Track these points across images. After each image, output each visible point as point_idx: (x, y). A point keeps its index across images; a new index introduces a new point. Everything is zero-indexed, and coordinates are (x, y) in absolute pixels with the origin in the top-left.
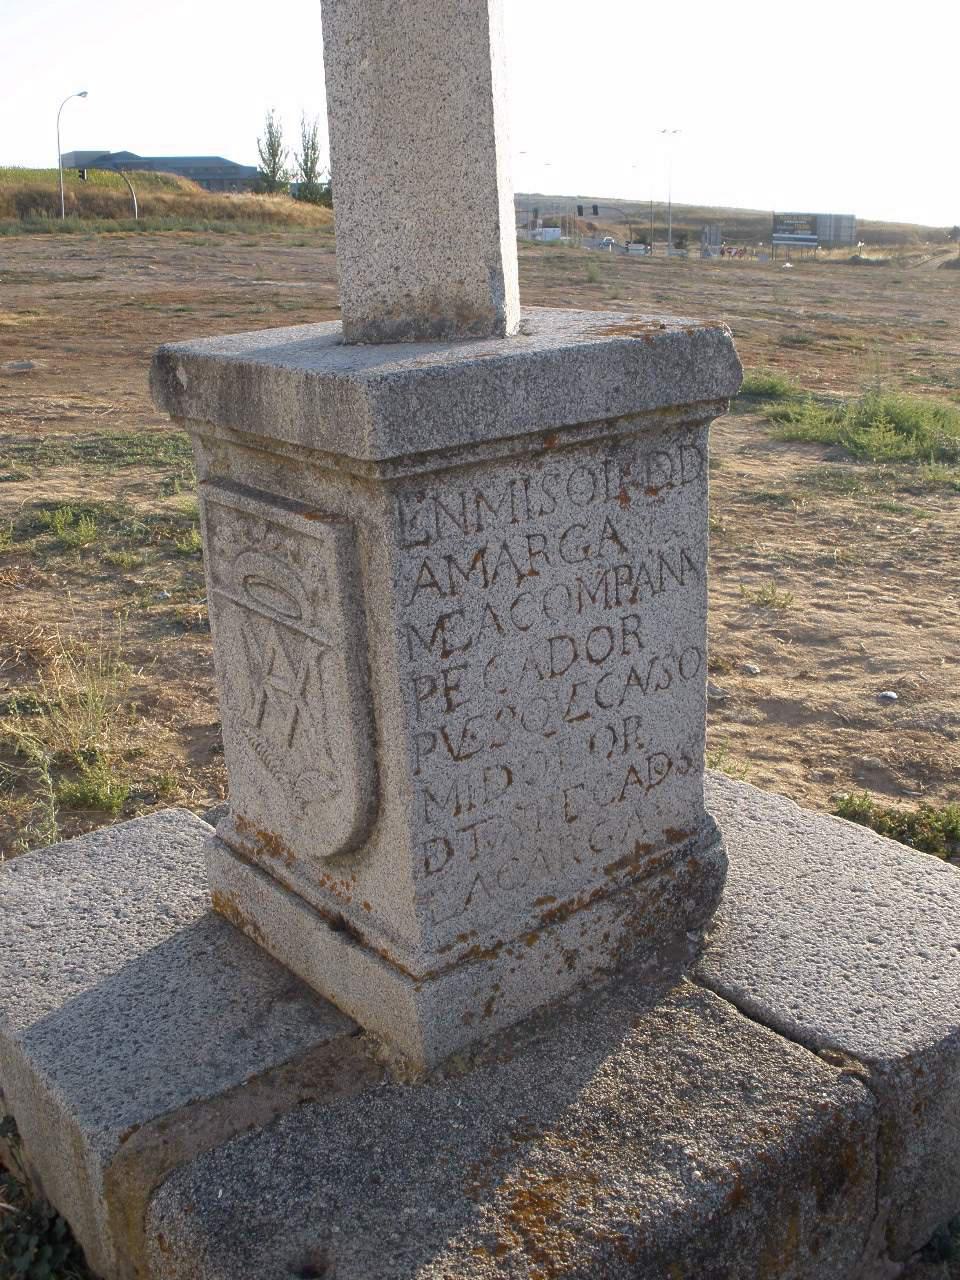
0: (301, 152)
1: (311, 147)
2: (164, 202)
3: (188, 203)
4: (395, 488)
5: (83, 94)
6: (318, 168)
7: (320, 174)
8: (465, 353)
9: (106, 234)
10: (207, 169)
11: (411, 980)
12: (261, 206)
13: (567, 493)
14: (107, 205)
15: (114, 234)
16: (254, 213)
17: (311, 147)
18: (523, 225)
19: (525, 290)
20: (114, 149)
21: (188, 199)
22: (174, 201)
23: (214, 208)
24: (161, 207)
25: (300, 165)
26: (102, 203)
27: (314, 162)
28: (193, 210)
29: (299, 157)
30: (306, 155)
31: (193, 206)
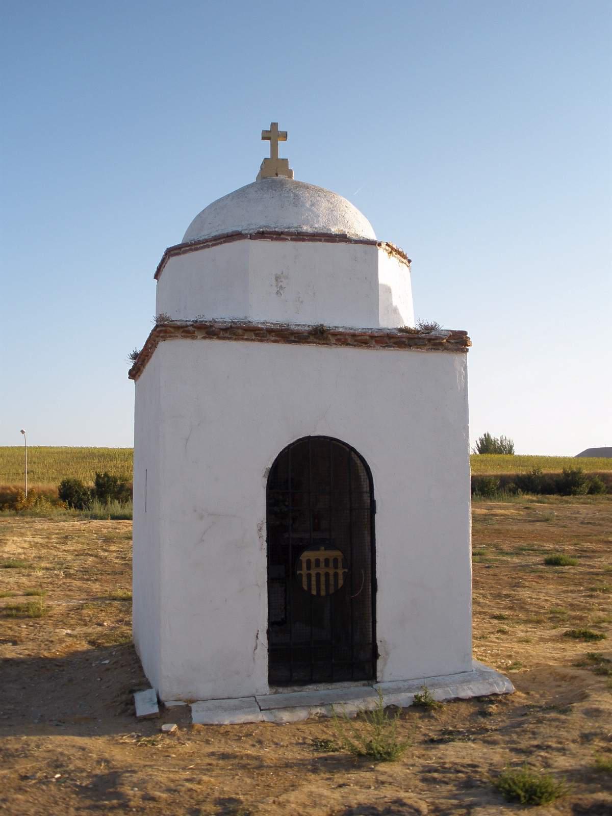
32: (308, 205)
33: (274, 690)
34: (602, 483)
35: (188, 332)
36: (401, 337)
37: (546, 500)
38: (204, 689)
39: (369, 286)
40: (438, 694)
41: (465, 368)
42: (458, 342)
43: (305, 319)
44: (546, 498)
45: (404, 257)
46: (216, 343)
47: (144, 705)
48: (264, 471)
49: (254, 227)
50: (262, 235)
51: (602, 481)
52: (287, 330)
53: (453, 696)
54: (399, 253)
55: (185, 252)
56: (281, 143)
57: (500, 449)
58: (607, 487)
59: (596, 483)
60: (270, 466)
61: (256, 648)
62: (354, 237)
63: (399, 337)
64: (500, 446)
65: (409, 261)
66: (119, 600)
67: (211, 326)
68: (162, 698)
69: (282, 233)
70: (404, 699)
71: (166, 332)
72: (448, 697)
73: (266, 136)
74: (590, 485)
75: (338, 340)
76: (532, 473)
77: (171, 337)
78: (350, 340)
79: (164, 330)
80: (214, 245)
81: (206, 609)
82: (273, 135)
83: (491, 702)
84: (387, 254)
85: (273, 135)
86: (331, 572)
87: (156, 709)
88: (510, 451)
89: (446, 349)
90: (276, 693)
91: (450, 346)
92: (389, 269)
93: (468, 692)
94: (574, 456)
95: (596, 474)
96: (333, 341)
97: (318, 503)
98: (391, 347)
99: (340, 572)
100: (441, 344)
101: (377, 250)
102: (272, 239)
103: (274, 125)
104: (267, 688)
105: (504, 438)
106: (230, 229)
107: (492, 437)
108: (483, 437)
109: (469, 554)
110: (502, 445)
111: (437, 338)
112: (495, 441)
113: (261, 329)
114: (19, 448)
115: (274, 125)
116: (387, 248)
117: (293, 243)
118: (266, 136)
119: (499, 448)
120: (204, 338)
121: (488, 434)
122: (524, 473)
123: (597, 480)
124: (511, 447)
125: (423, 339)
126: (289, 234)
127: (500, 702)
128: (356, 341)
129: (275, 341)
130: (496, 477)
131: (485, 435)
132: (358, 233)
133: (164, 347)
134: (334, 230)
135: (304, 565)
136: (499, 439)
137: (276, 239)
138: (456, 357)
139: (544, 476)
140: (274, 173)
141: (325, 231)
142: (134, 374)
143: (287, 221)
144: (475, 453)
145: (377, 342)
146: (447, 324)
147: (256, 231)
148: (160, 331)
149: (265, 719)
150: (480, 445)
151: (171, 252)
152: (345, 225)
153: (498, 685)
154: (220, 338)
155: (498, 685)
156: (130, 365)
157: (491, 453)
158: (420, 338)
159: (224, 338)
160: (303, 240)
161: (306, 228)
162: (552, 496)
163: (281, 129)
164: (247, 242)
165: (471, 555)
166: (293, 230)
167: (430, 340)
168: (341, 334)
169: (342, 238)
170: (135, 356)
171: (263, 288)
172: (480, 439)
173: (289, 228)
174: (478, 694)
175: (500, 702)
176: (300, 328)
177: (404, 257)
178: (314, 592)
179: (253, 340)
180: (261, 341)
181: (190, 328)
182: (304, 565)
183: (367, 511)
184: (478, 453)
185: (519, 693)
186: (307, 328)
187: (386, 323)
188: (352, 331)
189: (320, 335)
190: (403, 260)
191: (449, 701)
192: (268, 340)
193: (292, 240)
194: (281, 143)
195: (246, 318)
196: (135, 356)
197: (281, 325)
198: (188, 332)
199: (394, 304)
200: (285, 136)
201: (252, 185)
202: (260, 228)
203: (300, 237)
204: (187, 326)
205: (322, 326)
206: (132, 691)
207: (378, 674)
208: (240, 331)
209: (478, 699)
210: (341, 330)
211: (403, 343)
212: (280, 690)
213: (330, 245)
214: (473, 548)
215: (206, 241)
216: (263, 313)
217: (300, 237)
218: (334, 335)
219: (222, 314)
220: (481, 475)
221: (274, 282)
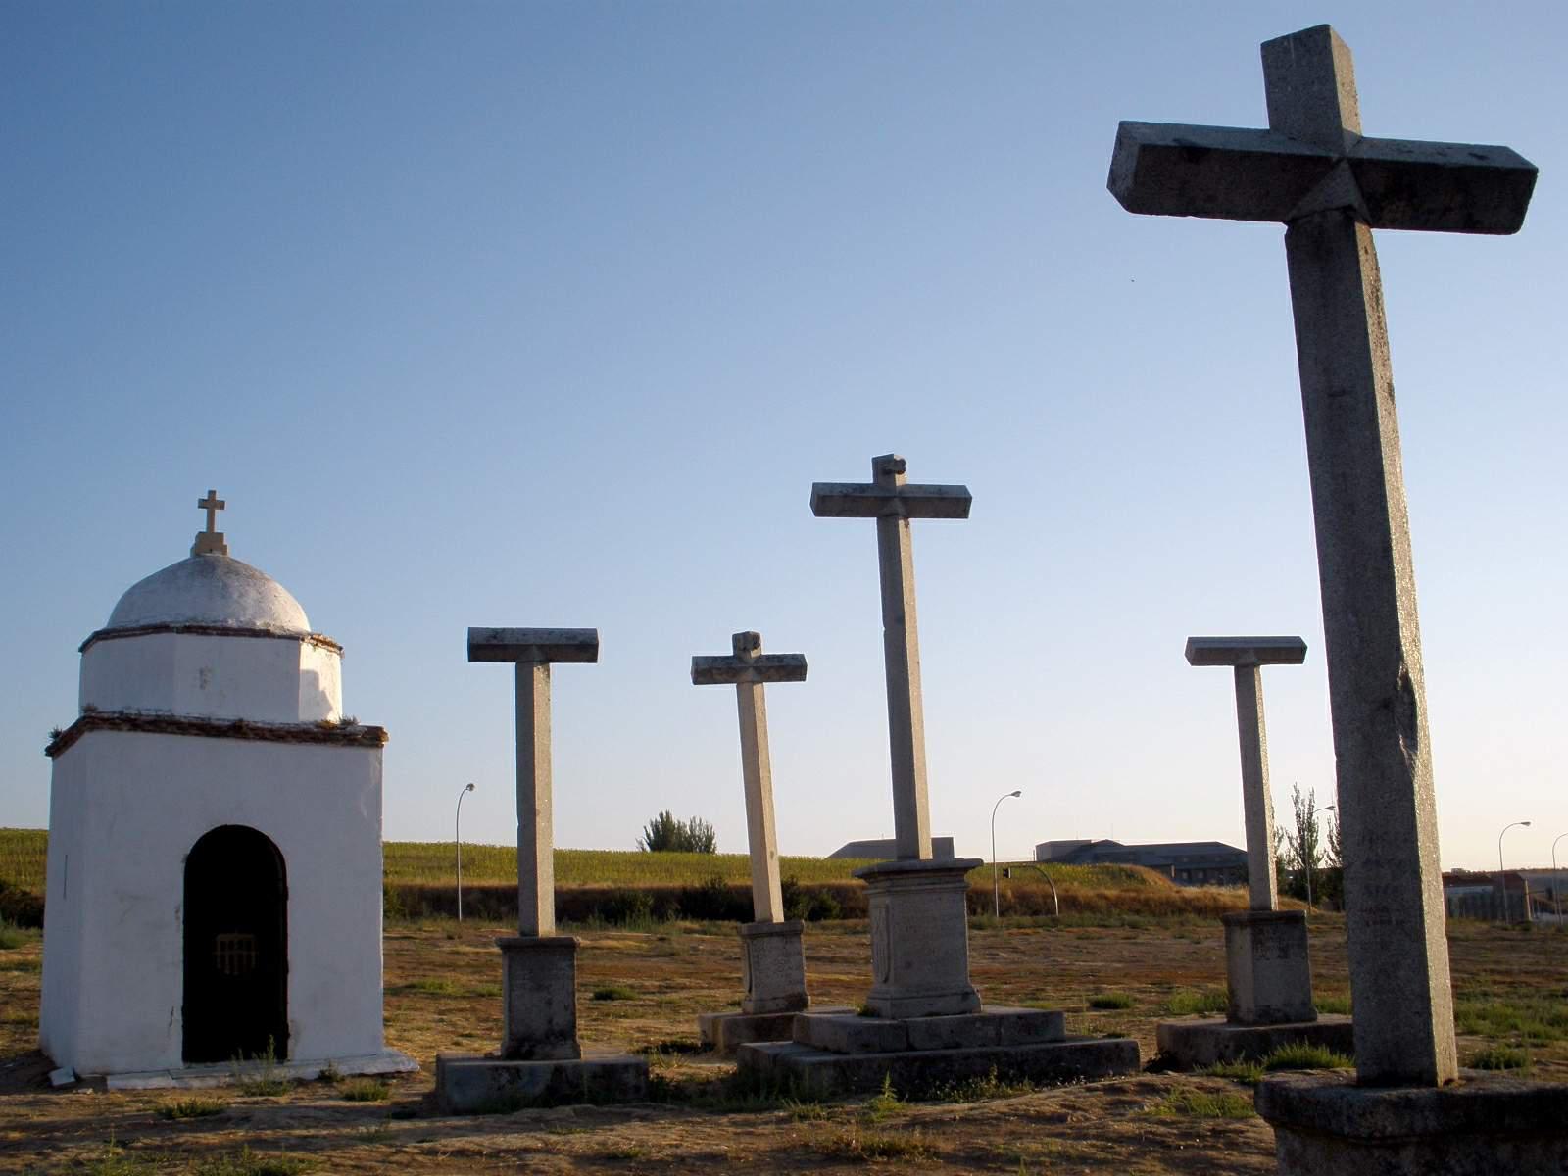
0: (1295, 833)
1: (1307, 828)
2: (1106, 898)
3: (1134, 899)
4: (751, 938)
5: (1017, 794)
6: (1318, 851)
7: (1319, 860)
8: (1310, 1024)
9: (1015, 931)
10: (1203, 857)
11: (830, 1046)
12: (1215, 899)
13: (776, 941)
14: (1045, 903)
15: (1022, 931)
16: (1207, 907)
17: (1307, 828)
18: (1456, 909)
19: (1457, 975)
20: (1095, 837)
21: (1133, 894)
22: (1118, 897)
23: (1162, 903)
24: (1102, 903)
25: (1296, 849)
26: (1040, 900)
27: (1312, 847)
28: (1138, 907)
29: (1294, 841)
30: (1302, 838)
31: (1139, 901)
32: (236, 596)
33: (187, 1066)
34: (835, 903)
35: (114, 724)
36: (317, 733)
37: (714, 930)
38: (119, 1064)
39: (291, 677)
40: (343, 1070)
41: (381, 764)
42: (374, 737)
43: (226, 714)
44: (716, 926)
45: (333, 645)
46: (141, 736)
47: (58, 1078)
48: (182, 856)
49: (181, 620)
50: (188, 630)
51: (834, 898)
52: (209, 724)
53: (358, 1072)
54: (325, 643)
55: (114, 637)
56: (217, 512)
57: (690, 843)
58: (842, 909)
59: (823, 902)
60: (189, 852)
61: (170, 1024)
62: (278, 632)
63: (314, 733)
64: (690, 837)
65: (341, 648)
66: (11, 1024)
67: (136, 720)
68: (78, 1071)
69: (208, 628)
70: (311, 1072)
71: (93, 723)
72: (353, 1072)
73: (203, 504)
74: (810, 907)
75: (256, 735)
76: (710, 885)
77: (98, 728)
78: (267, 735)
79: (91, 721)
80: (141, 635)
81: (117, 990)
82: (211, 504)
83: (394, 1078)
84: (311, 647)
85: (211, 504)
86: (245, 953)
87: (73, 1079)
88: (707, 845)
89: (361, 744)
90: (189, 1068)
91: (365, 741)
92: (311, 658)
93: (373, 1069)
94: (826, 857)
95: (822, 887)
96: (251, 736)
97: (235, 891)
98: (306, 741)
99: (253, 954)
100: (355, 740)
101: (300, 645)
102: (198, 633)
103: (212, 493)
104: (181, 1064)
105: (697, 822)
106: (157, 621)
107: (675, 820)
108: (659, 820)
109: (379, 940)
110: (693, 835)
111: (351, 734)
112: (679, 826)
113: (182, 723)
114: (446, 846)
115: (212, 493)
116: (312, 641)
117: (218, 637)
118: (203, 504)
119: (688, 840)
120: (130, 730)
121: (668, 814)
122: (697, 885)
123: (826, 897)
124: (710, 839)
125: (337, 734)
126: (215, 629)
127: (402, 1078)
128: (274, 735)
129: (197, 735)
130: (648, 892)
131: (661, 816)
132: (285, 625)
133: (88, 738)
134: (259, 624)
135: (219, 947)
136: (688, 824)
137: (202, 634)
138: (372, 752)
139: (729, 891)
140: (209, 543)
141: (248, 627)
142: (52, 751)
143: (214, 614)
144: (643, 849)
145: (294, 737)
146: (365, 721)
147: (183, 625)
148: (88, 723)
149: (177, 1085)
150: (652, 835)
151: (99, 636)
152: (272, 617)
153: (403, 1064)
154: (144, 730)
155: (403, 1064)
156: (49, 742)
157: (674, 850)
158: (334, 734)
159: (149, 731)
160: (228, 635)
161: (232, 623)
162: (726, 923)
163: (218, 497)
164: (174, 635)
165: (382, 940)
166: (218, 625)
167: (345, 736)
168: (258, 729)
169: (266, 634)
170: (56, 735)
171: (189, 681)
172: (651, 825)
173: (214, 622)
174: (382, 1071)
175: (402, 1078)
176: (220, 722)
177: (333, 645)
178: (228, 972)
179: (175, 733)
180: (183, 734)
181: (117, 721)
182: (219, 947)
183: (282, 895)
184: (648, 849)
185: (424, 1074)
186: (227, 723)
187: (305, 715)
188: (269, 727)
189: (238, 730)
190: (332, 649)
191: (353, 1076)
192: (191, 734)
193: (217, 634)
194: (217, 512)
195: (169, 711)
196: (56, 735)
197: (202, 720)
198: (114, 724)
199: (321, 688)
200: (222, 505)
201: (182, 565)
202: (187, 621)
203: (225, 632)
204: (113, 719)
205: (241, 721)
206: (48, 1072)
207: (289, 1053)
208: (164, 725)
209: (382, 1076)
210: (259, 725)
211: (319, 739)
212: (194, 1065)
213: (253, 640)
214: (384, 930)
215: (134, 629)
216: (188, 706)
217: (225, 632)
218: (252, 729)
219: (148, 705)
220: (620, 888)
221: (198, 675)
